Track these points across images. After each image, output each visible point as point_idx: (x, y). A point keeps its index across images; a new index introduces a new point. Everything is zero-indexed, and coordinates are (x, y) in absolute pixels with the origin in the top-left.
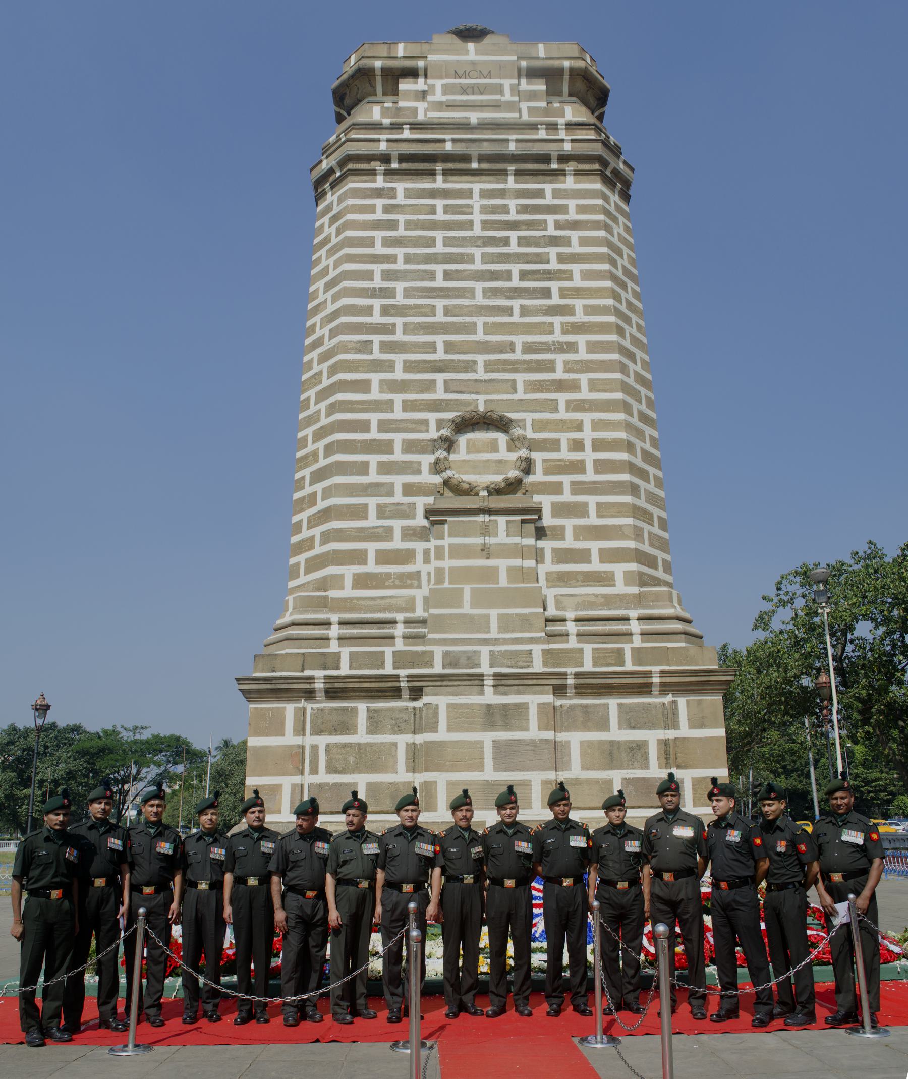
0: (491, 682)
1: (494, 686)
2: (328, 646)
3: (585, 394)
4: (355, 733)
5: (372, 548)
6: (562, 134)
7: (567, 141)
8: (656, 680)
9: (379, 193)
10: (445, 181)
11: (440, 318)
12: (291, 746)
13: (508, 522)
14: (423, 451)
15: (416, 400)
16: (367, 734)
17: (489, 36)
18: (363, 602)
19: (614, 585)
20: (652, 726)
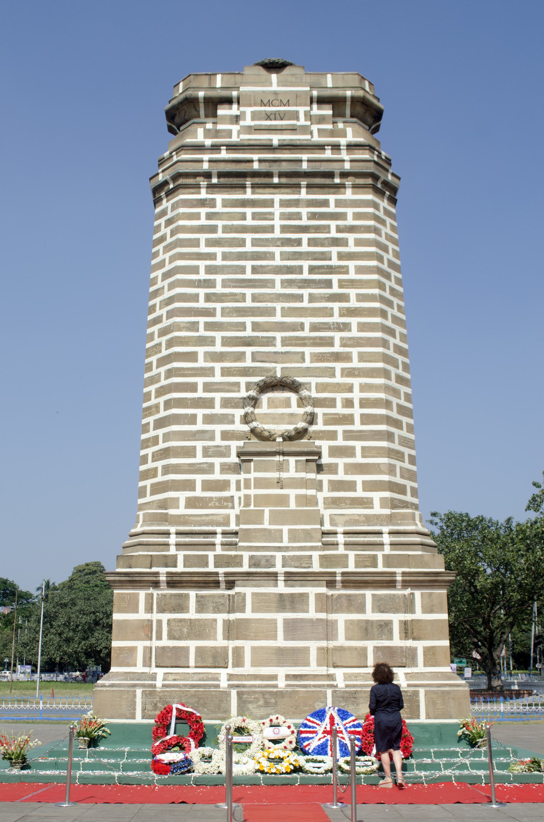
0: (283, 578)
1: (285, 580)
2: (169, 550)
3: (355, 364)
4: (188, 611)
5: (199, 478)
9: (202, 203)
10: (253, 193)
11: (249, 303)
14: (236, 406)
15: (231, 368)
16: (196, 612)
19: (372, 508)
20: (396, 611)
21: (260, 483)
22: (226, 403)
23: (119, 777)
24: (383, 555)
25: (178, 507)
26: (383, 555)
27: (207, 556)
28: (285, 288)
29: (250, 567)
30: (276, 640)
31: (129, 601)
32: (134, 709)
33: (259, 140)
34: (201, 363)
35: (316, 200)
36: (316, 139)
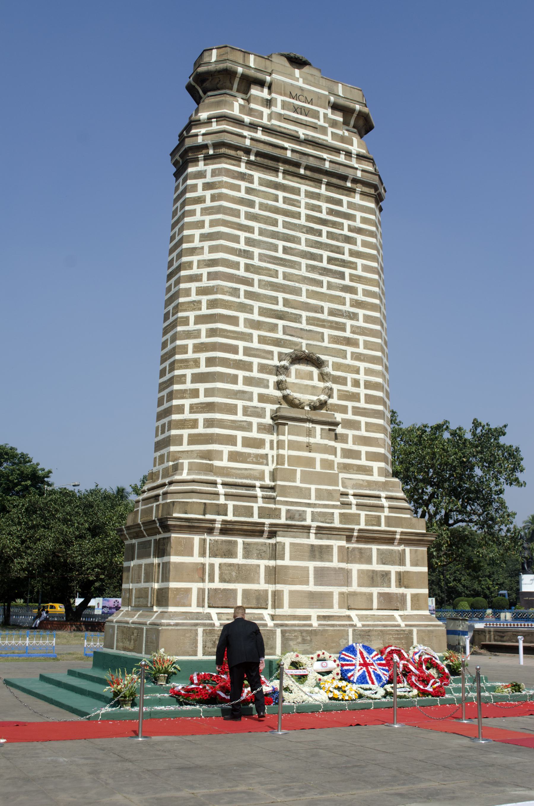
0: (314, 531)
1: (315, 533)
2: (218, 499)
4: (236, 557)
5: (240, 435)
6: (354, 163)
7: (360, 170)
8: (398, 537)
9: (242, 177)
11: (280, 280)
12: (198, 564)
14: (270, 373)
15: (266, 337)
16: (243, 558)
17: (307, 67)
18: (234, 471)
20: (393, 563)
21: (293, 445)
22: (263, 368)
23: (418, 701)
25: (222, 460)
26: (259, 507)
27: (252, 507)
28: (309, 272)
29: (287, 519)
30: (308, 585)
31: (185, 545)
32: (196, 647)
33: (288, 129)
34: (241, 328)
35: (333, 197)
36: (328, 139)
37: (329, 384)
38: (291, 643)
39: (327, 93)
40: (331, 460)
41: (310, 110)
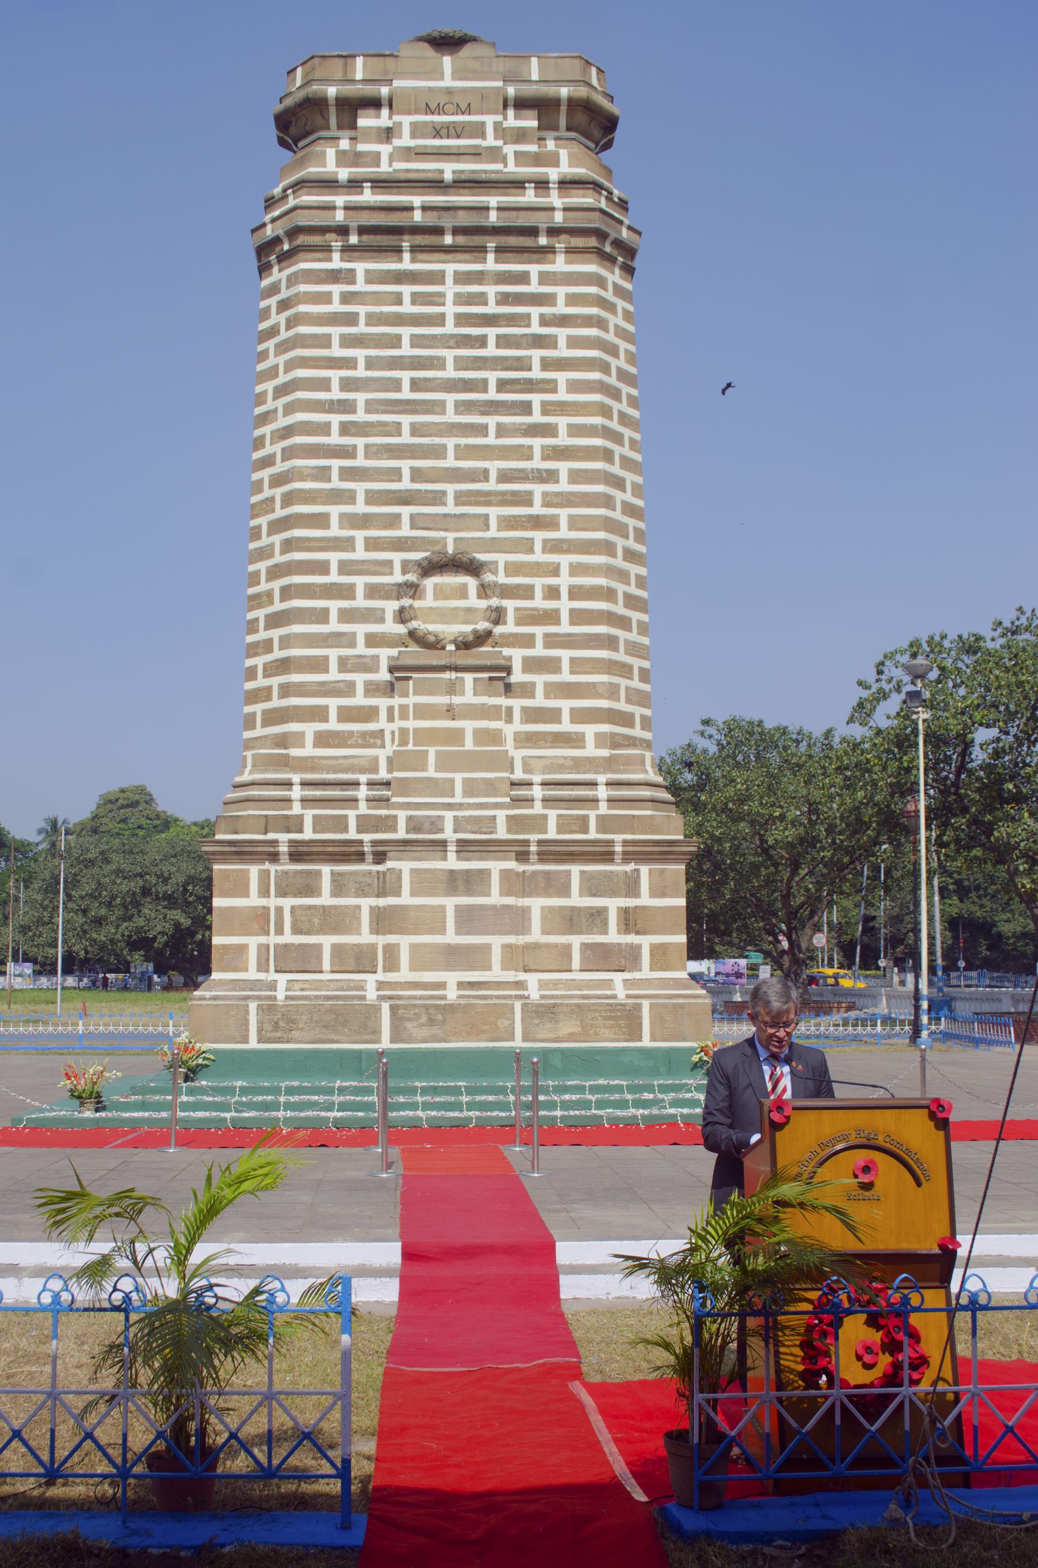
0: (455, 849)
2: (291, 808)
3: (564, 533)
4: (319, 895)
5: (333, 704)
9: (335, 276)
13: (475, 680)
14: (387, 597)
15: (379, 538)
17: (469, 45)
19: (584, 747)
20: (613, 893)
21: (422, 712)
24: (597, 816)
25: (303, 746)
28: (461, 414)
29: (408, 832)
32: (247, 1030)
33: (423, 171)
34: (335, 530)
35: (509, 272)
36: (512, 169)
37: (494, 602)
38: (409, 1025)
39: (500, 84)
40: (496, 730)
41: (464, 125)
